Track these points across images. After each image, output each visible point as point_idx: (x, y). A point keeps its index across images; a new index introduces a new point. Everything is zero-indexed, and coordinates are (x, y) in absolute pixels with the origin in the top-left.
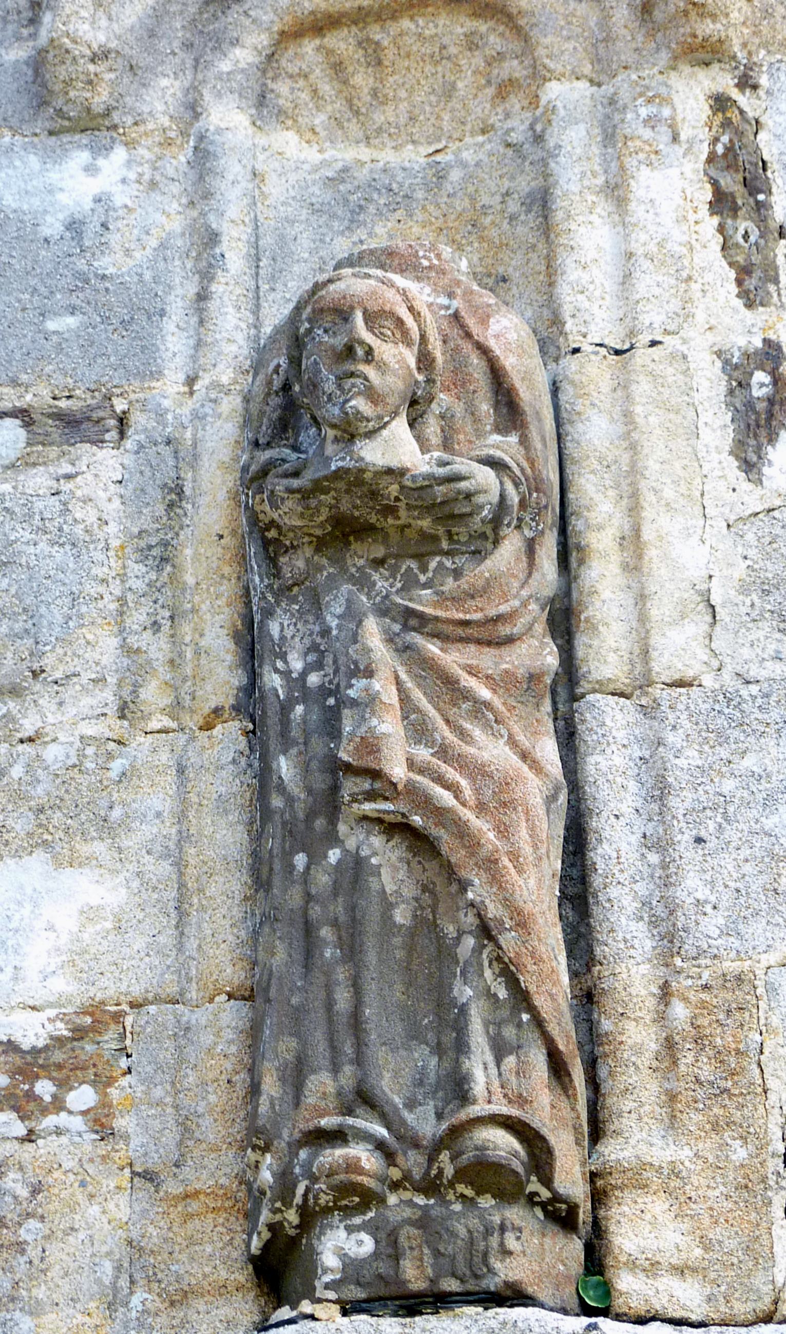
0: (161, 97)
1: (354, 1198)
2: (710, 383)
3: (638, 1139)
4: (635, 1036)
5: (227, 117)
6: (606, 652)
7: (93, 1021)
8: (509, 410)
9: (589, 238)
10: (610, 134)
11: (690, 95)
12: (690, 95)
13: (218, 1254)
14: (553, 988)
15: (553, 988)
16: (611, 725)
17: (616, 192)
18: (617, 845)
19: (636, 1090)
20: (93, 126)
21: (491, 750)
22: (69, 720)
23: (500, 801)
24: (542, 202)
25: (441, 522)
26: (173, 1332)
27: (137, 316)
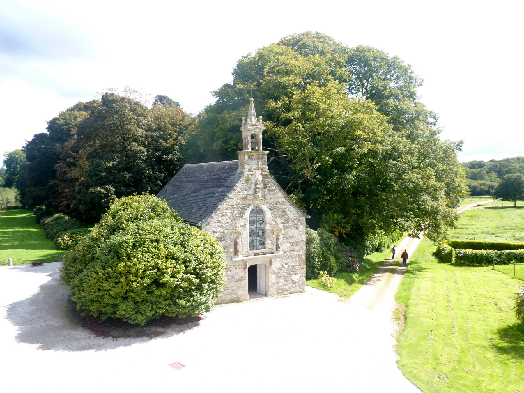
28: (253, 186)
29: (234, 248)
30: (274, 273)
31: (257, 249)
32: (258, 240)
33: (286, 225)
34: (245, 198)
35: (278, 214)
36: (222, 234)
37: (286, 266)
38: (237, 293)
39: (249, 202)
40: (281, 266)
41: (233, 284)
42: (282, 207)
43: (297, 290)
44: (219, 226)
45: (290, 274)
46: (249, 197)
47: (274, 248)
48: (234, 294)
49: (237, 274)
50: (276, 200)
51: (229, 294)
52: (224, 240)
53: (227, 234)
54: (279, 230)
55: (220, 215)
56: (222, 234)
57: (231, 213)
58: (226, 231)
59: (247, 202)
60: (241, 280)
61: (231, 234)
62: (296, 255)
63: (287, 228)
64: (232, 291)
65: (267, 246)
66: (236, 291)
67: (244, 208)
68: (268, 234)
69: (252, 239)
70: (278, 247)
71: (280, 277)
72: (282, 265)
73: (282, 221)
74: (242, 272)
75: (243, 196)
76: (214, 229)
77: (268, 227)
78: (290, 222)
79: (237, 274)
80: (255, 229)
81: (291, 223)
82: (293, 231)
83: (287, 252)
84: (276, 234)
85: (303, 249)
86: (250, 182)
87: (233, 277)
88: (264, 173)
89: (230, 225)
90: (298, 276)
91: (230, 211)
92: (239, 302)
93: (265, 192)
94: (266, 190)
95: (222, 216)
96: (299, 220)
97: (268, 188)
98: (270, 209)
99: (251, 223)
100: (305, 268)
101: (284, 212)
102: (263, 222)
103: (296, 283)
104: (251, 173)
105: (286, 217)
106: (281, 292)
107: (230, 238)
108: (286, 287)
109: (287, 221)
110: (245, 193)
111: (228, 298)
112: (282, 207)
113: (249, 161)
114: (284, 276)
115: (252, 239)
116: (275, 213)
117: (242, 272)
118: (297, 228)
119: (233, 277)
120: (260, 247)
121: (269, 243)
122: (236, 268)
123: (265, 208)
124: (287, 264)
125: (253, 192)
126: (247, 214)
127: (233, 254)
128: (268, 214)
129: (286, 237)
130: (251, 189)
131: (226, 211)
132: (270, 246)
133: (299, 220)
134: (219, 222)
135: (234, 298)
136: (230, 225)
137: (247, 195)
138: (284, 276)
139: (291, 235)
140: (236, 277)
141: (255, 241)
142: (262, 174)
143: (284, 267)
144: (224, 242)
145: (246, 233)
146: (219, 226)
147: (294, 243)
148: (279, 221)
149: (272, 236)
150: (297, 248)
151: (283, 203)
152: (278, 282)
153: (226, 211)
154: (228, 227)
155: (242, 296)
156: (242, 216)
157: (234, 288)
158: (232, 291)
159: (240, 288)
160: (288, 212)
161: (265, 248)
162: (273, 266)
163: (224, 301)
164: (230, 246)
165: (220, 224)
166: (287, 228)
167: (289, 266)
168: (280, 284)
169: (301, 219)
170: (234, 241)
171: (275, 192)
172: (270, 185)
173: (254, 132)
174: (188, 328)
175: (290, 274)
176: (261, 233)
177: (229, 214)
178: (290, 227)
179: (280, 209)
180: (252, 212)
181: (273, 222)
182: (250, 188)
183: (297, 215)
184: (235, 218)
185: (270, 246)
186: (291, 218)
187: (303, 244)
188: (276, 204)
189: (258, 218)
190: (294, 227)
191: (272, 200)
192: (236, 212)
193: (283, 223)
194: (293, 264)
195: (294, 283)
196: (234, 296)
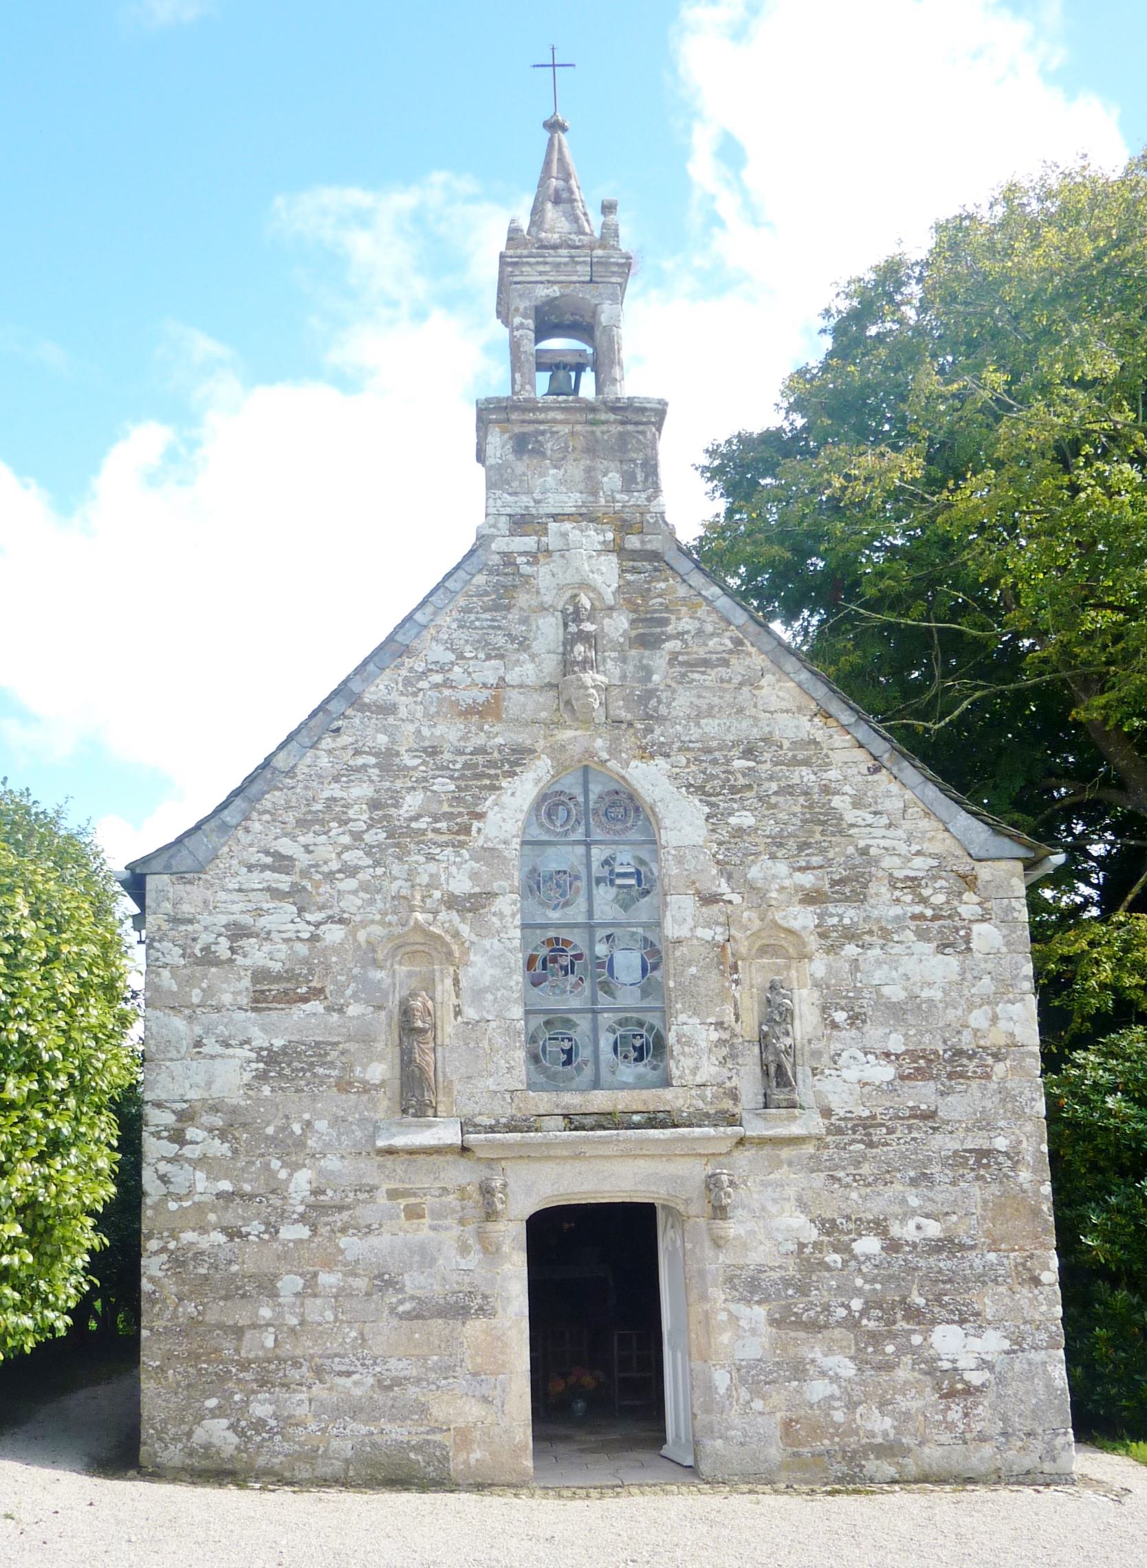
0: (388, 964)
1: (413, 1106)
2: (452, 1008)
3: (440, 1098)
4: (441, 1086)
5: (396, 967)
6: (439, 1041)
7: (383, 1081)
8: (430, 1014)
9: (439, 988)
10: (441, 972)
11: (451, 969)
12: (451, 969)
13: (398, 1108)
14: (433, 1086)
15: (433, 1086)
16: (439, 1049)
17: (442, 981)
18: (439, 1064)
19: (441, 1092)
20: (381, 968)
21: (427, 1058)
22: (379, 1046)
23: (428, 1065)
24: (434, 980)
25: (422, 1031)
26: (736, 1564)
27: (387, 994)
28: (548, 631)
29: (393, 1054)
30: (750, 1286)
31: (596, 1084)
32: (607, 1019)
33: (850, 914)
34: (488, 710)
35: (771, 827)
36: (302, 949)
37: (869, 1245)
38: (424, 1409)
39: (522, 738)
40: (812, 1234)
41: (384, 1333)
42: (805, 775)
43: (983, 1457)
44: (275, 893)
45: (913, 1314)
46: (515, 702)
47: (748, 1082)
48: (399, 1414)
49: (426, 1257)
50: (743, 729)
51: (356, 1411)
52: (318, 993)
53: (337, 949)
54: (779, 945)
55: (290, 818)
56: (302, 949)
57: (374, 805)
58: (333, 934)
59: (500, 736)
60: (458, 1309)
61: (369, 955)
62: (957, 1160)
63: (850, 934)
64: (383, 1386)
65: (680, 1065)
66: (412, 1391)
67: (485, 773)
68: (687, 969)
69: (548, 999)
70: (777, 1076)
71: (814, 1327)
72: (828, 1227)
73: (807, 880)
74: (464, 1250)
75: (467, 697)
76: (237, 910)
77: (681, 919)
78: (880, 890)
79: (426, 1257)
80: (577, 938)
81: (885, 904)
82: (908, 965)
83: (866, 1124)
84: (756, 975)
85: (1019, 1115)
86: (523, 599)
87: (385, 1282)
88: (633, 542)
89: (365, 887)
90: (993, 1343)
91: (362, 791)
92: (441, 1483)
93: (648, 672)
94: (659, 661)
95: (302, 824)
96: (968, 881)
97: (669, 645)
98: (700, 790)
99: (536, 884)
100: (1051, 1276)
101: (822, 818)
102: (642, 884)
103: (969, 1391)
104: (529, 543)
105: (841, 852)
106: (838, 1465)
107: (364, 981)
108: (880, 1424)
109: (852, 885)
110: (489, 672)
111: (345, 1439)
112: (805, 775)
113: (520, 467)
114: (851, 1323)
115: (548, 999)
116: (745, 819)
117: (464, 1250)
118: (953, 940)
119: (385, 1282)
120: (628, 1072)
121: (702, 1053)
122: (414, 1213)
123: (649, 779)
124: (879, 1227)
125: (551, 664)
126: (509, 810)
127: (384, 1103)
128: (683, 824)
129: (849, 1008)
130: (537, 646)
131: (335, 791)
132: (709, 1070)
133: (968, 881)
134: (282, 863)
135: (403, 1447)
136: (365, 887)
137: (502, 683)
138: (851, 1323)
139: (895, 993)
140: (414, 1282)
141: (583, 1024)
142: (620, 550)
143: (844, 1248)
144: (315, 1006)
145: (492, 963)
146: (275, 893)
147: (930, 1057)
148: (775, 873)
149: (724, 995)
150: (958, 1106)
151: (809, 753)
152: (799, 1370)
153: (335, 791)
154: (351, 904)
155: (464, 1438)
156: (466, 830)
157: (397, 1367)
158: (383, 1386)
159: (447, 1370)
160: (850, 816)
161: (667, 1083)
162: (732, 1228)
163: (310, 1456)
164: (366, 1039)
165: (283, 882)
166: (850, 934)
167: (893, 1246)
168: (818, 1389)
169: (985, 872)
170: (393, 1004)
171: (738, 667)
172: (687, 624)
173: (555, 291)
174: (220, 1485)
175: (913, 1314)
176: (628, 963)
177: (360, 816)
178: (886, 934)
179: (788, 790)
180: (550, 804)
181: (724, 887)
182: (523, 644)
183: (941, 844)
184: (401, 837)
185: (709, 1070)
186: (887, 862)
187: (1017, 1069)
188: (749, 753)
189: (598, 854)
190: (922, 935)
191: (711, 726)
192: (412, 802)
193: (811, 898)
194: (933, 1229)
195: (952, 1388)
196: (396, 1432)
